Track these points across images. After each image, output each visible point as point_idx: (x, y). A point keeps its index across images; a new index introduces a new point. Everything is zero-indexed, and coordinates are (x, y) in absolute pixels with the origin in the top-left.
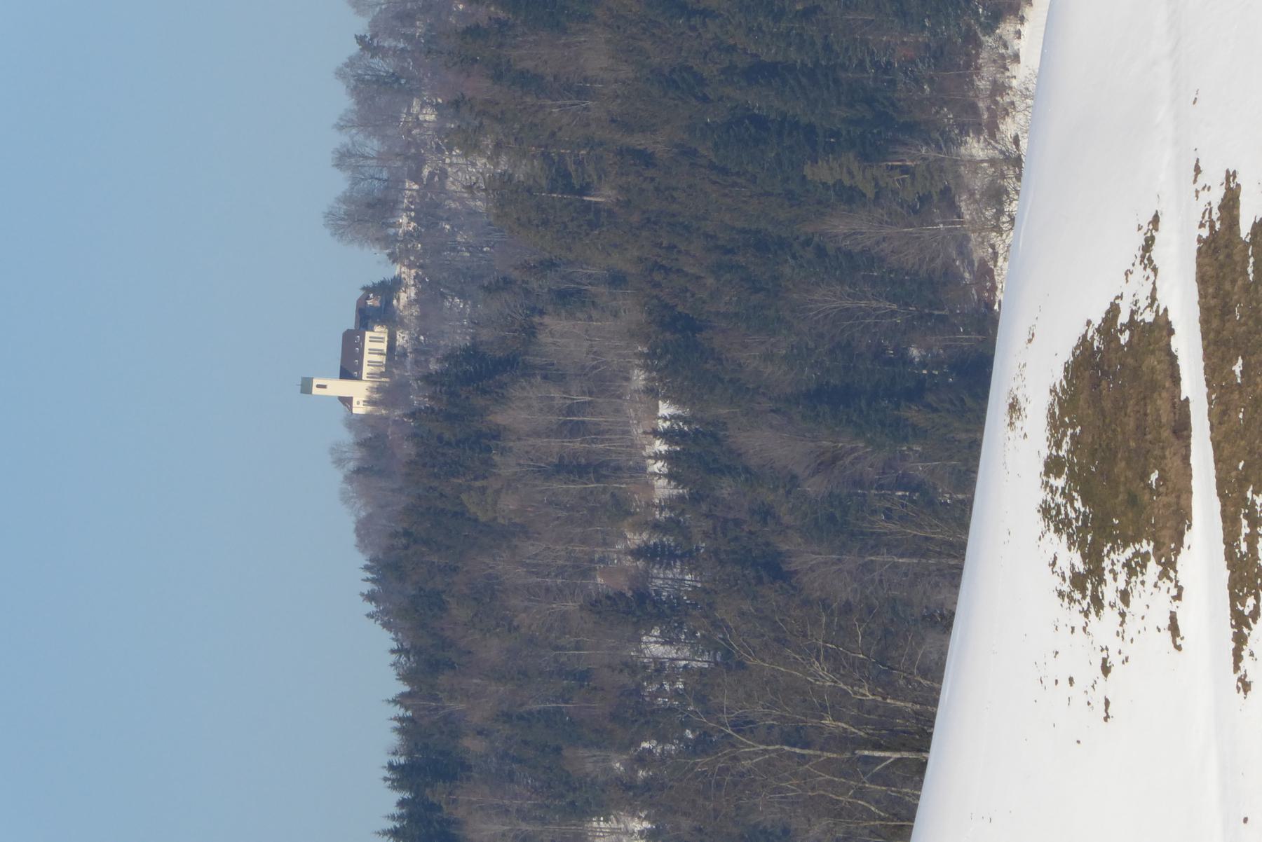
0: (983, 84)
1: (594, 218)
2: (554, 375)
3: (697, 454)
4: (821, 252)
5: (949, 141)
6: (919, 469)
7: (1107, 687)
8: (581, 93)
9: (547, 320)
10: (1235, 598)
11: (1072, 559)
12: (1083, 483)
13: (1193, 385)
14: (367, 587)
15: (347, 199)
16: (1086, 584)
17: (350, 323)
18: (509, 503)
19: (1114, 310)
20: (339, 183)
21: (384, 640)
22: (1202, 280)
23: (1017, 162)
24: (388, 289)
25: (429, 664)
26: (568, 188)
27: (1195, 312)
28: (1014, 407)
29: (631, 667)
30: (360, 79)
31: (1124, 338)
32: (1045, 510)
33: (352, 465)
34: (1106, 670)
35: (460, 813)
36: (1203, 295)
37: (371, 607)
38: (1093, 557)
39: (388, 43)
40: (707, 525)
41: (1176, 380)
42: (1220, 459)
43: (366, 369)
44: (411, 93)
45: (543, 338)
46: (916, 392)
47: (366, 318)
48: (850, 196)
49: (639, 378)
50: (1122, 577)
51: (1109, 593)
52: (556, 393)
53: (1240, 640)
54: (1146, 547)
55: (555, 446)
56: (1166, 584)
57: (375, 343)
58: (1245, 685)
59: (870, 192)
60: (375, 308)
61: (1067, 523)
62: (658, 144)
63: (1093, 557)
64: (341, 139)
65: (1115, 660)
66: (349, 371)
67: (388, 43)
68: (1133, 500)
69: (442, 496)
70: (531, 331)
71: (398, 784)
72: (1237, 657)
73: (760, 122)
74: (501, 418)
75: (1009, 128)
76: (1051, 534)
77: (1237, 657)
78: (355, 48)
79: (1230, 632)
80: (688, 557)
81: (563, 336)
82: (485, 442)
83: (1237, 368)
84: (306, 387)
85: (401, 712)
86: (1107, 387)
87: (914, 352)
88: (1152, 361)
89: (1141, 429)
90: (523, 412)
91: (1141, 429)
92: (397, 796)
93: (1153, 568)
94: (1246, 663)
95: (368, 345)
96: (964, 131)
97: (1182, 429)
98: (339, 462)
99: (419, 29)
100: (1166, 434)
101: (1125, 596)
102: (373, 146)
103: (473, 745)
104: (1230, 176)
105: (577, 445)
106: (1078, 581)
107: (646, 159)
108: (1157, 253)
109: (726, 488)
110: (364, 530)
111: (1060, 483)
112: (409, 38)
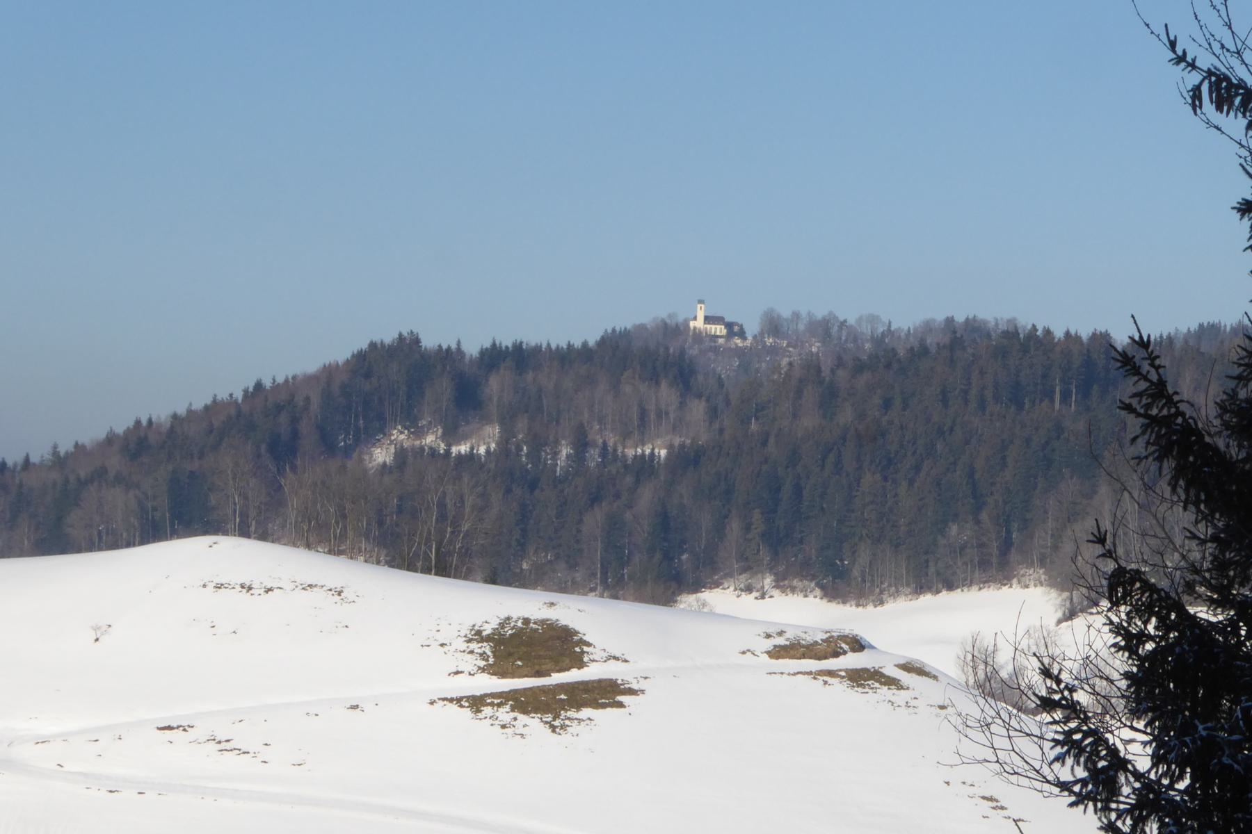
0: (795, 582)
1: (745, 422)
2: (682, 405)
3: (645, 466)
4: (726, 517)
5: (771, 569)
6: (636, 559)
7: (435, 645)
8: (795, 416)
9: (704, 403)
10: (468, 698)
11: (488, 630)
12: (519, 634)
13: (557, 678)
14: (618, 329)
15: (779, 317)
16: (479, 636)
17: (728, 319)
18: (627, 389)
19: (589, 645)
20: (786, 313)
21: (593, 339)
22: (600, 681)
23: (763, 597)
24: (742, 334)
25: (566, 358)
26: (757, 411)
27: (587, 679)
28: (552, 604)
29: (557, 442)
30: (828, 321)
31: (577, 649)
32: (508, 618)
33: (668, 321)
34: (442, 645)
35: (502, 371)
36: (593, 681)
37: (610, 331)
38: (488, 639)
39: (844, 333)
40: (614, 471)
41: (559, 671)
42: (525, 691)
43: (708, 326)
44: (823, 342)
45: (696, 401)
46: (668, 557)
47: (729, 326)
48: (748, 528)
49: (677, 441)
50: (480, 651)
51: (474, 646)
52: (674, 407)
53: (451, 700)
54: (491, 660)
55: (652, 408)
56: (475, 669)
57: (719, 330)
58: (432, 703)
59: (749, 536)
60: (734, 330)
61: (503, 628)
62: (771, 448)
63: (488, 639)
64: (804, 313)
65: (446, 649)
66: (708, 319)
67: (844, 333)
68: (510, 654)
69: (649, 361)
70: (699, 396)
71: (514, 345)
72: (444, 699)
73: (778, 490)
74: (664, 385)
75: (776, 593)
76: (498, 621)
77: (444, 699)
78: (842, 319)
79: (454, 696)
80: (603, 464)
81: (698, 409)
82: (654, 378)
83: (563, 697)
84: (701, 302)
85: (544, 346)
86: (558, 643)
87: (685, 557)
88: (567, 661)
89: (540, 657)
90: (667, 394)
91: (540, 657)
92: (510, 345)
93: (482, 663)
94: (441, 703)
95: (718, 327)
96: (775, 574)
97: (539, 674)
98: (670, 316)
99: (851, 345)
100: (537, 667)
101: (472, 652)
102: (801, 327)
103: (530, 376)
104: (643, 692)
105: (653, 416)
106: (479, 633)
107: (765, 443)
108: (612, 662)
109: (629, 480)
110: (641, 328)
111: (519, 624)
112: (846, 341)
